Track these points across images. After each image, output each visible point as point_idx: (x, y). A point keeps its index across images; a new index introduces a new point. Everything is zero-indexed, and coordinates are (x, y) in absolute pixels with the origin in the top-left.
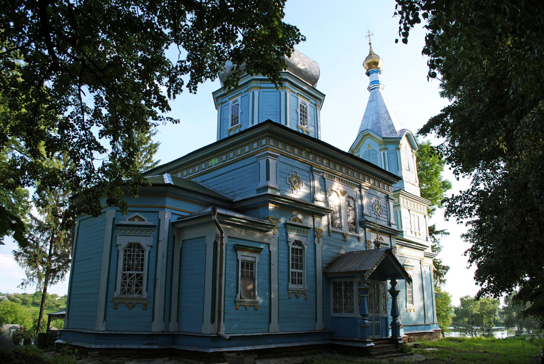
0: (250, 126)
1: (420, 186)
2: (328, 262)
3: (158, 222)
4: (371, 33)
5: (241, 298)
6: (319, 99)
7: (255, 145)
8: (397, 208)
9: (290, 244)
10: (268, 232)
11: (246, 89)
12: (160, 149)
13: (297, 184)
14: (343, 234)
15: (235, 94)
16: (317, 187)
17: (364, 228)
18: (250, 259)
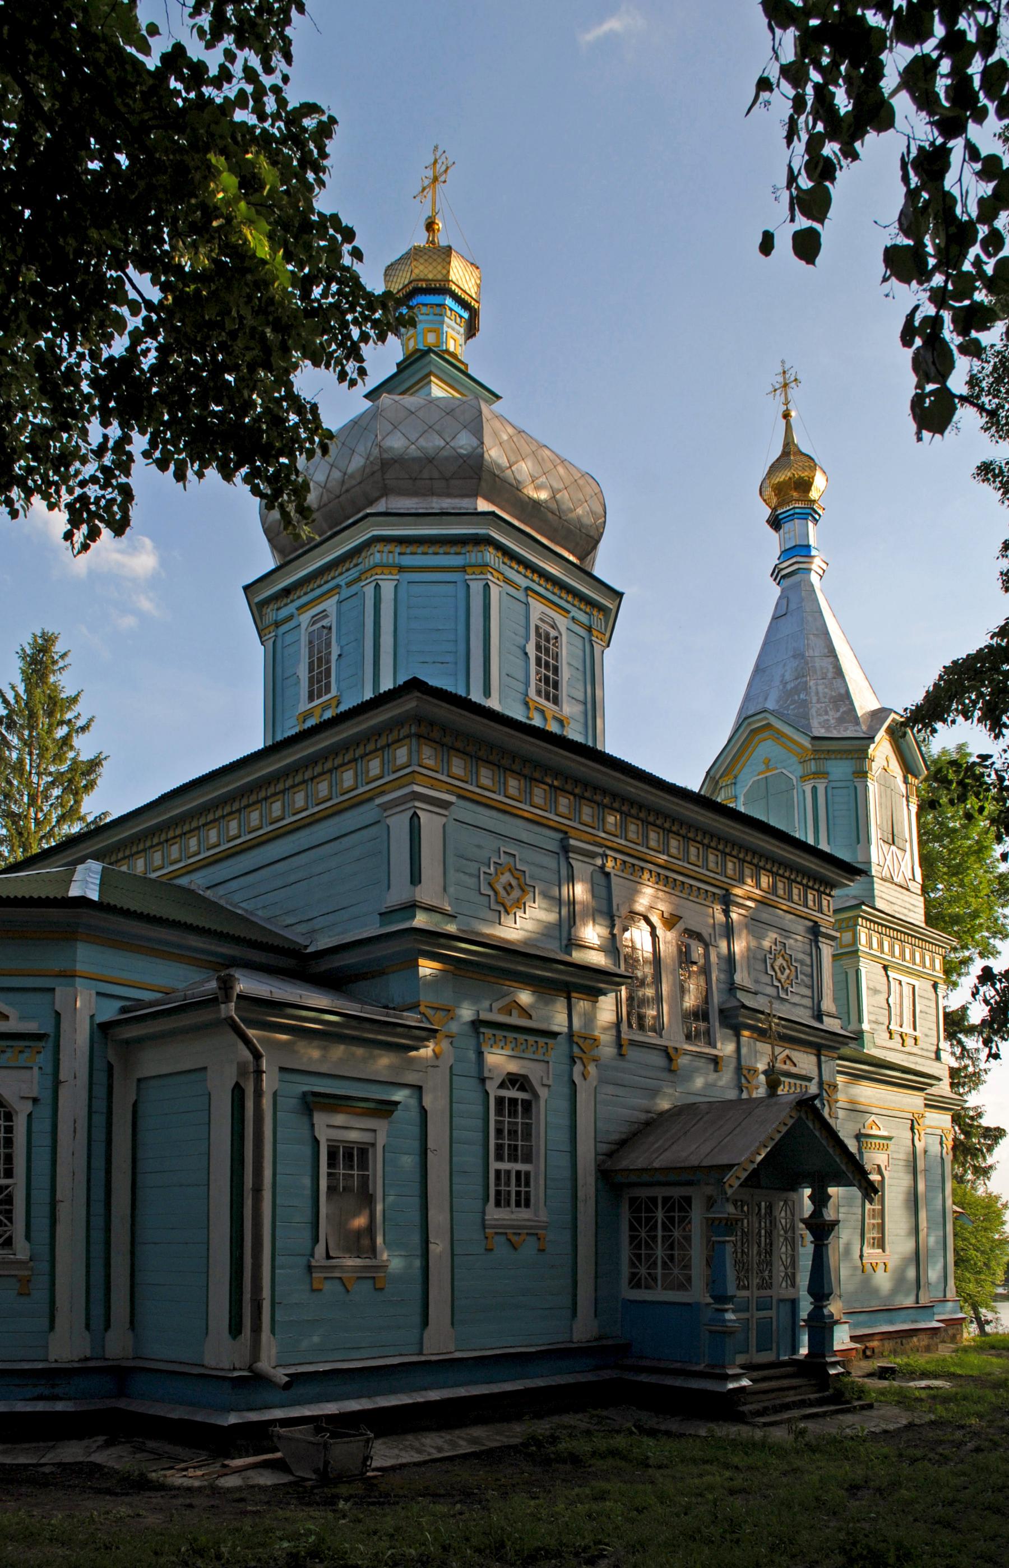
0: (368, 695)
1: (924, 890)
2: (615, 1137)
3: (52, 1021)
4: (790, 376)
5: (328, 1257)
6: (600, 605)
7: (375, 766)
8: (846, 962)
9: (492, 1087)
10: (417, 1049)
11: (353, 574)
12: (105, 775)
13: (516, 893)
14: (665, 1050)
15: (318, 592)
16: (582, 903)
17: (737, 1031)
18: (353, 1136)
